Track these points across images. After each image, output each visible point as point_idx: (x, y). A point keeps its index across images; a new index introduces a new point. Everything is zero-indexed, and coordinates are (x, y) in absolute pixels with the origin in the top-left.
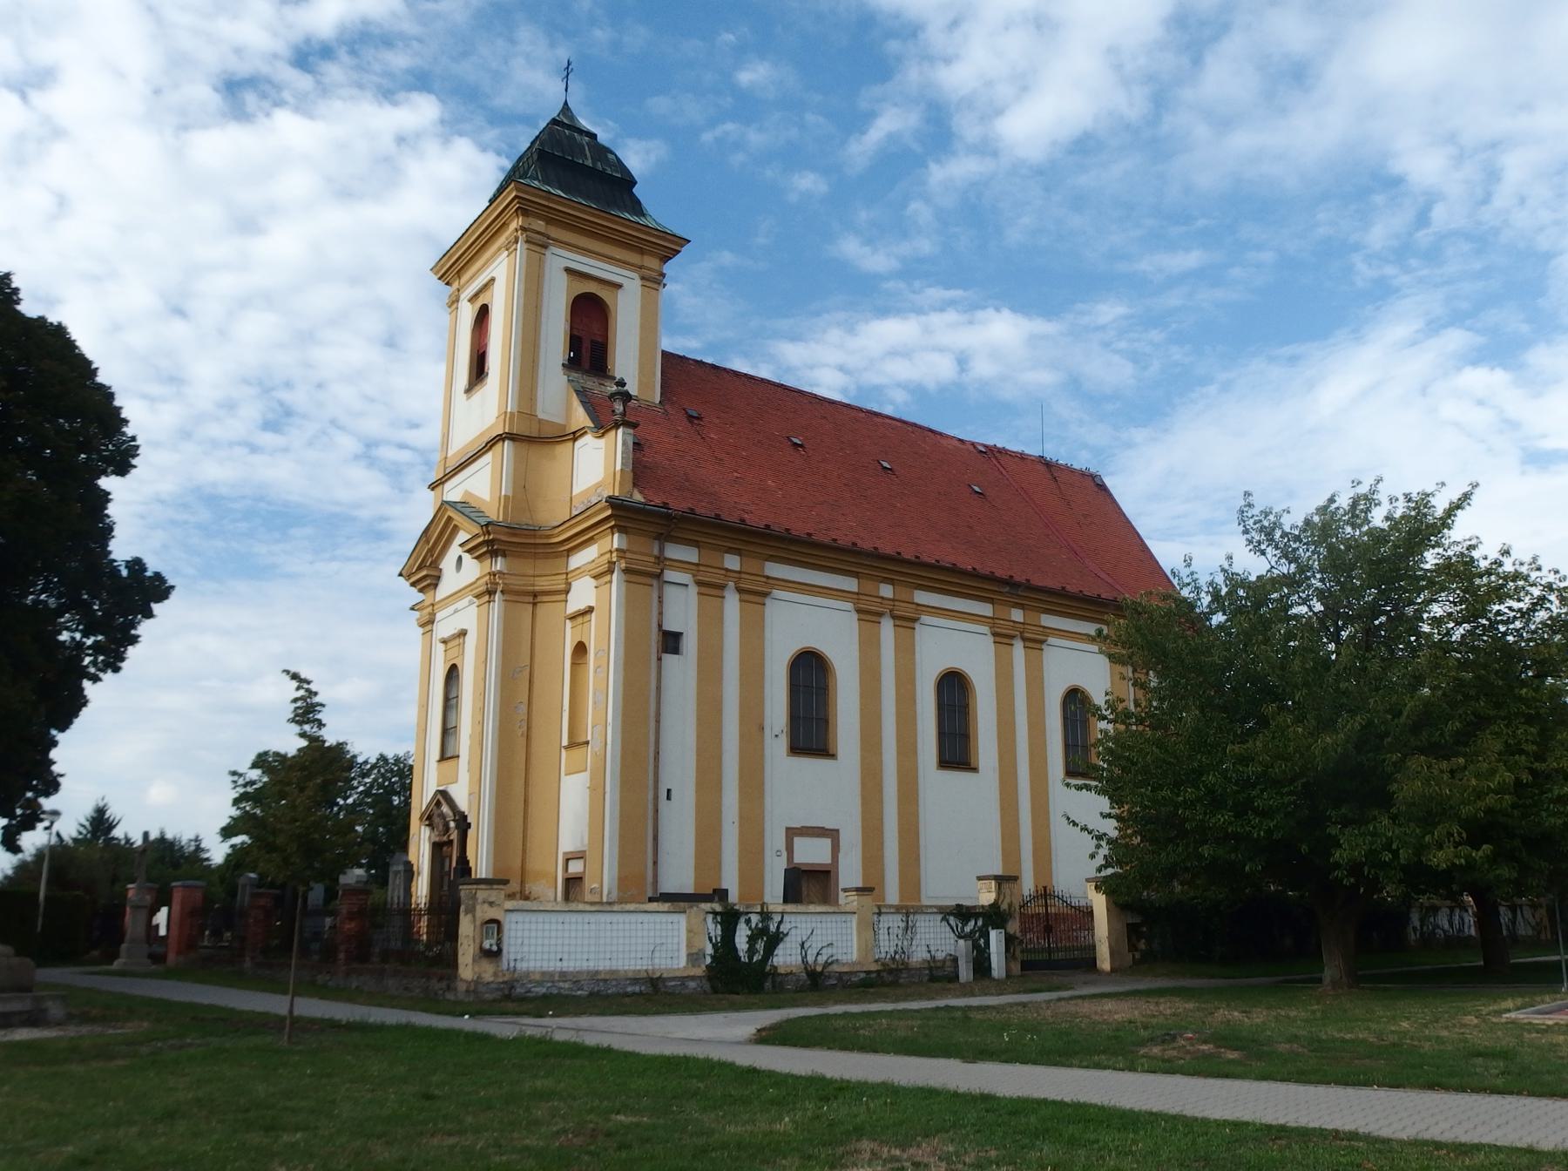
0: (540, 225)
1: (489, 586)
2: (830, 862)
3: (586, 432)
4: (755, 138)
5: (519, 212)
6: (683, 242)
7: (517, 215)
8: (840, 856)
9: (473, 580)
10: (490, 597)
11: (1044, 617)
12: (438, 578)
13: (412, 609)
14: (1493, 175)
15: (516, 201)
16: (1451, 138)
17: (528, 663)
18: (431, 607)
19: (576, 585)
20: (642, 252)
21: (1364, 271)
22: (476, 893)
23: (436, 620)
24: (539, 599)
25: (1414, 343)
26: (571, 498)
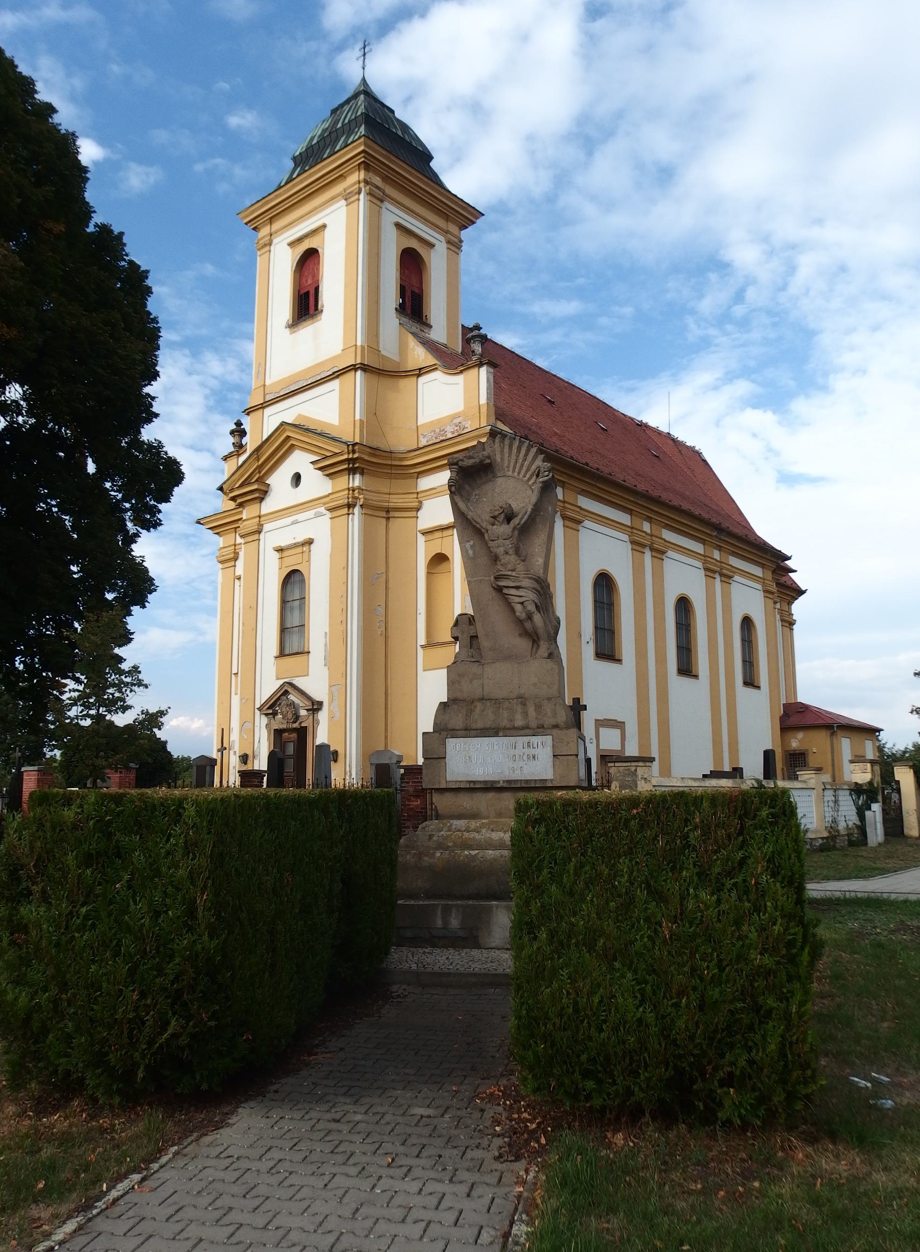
0: (377, 180)
1: (350, 500)
2: (620, 749)
3: (437, 368)
4: (239, 172)
5: (362, 166)
6: (477, 214)
7: (359, 169)
8: (626, 743)
9: (327, 493)
10: (349, 510)
11: (730, 557)
12: (266, 492)
13: (198, 522)
14: (791, 269)
15: (362, 155)
16: (765, 239)
17: (384, 571)
18: (258, 519)
19: (428, 505)
20: (447, 218)
21: (694, 332)
22: (636, 770)
23: (264, 530)
24: (392, 514)
25: (716, 388)
26: (417, 427)
